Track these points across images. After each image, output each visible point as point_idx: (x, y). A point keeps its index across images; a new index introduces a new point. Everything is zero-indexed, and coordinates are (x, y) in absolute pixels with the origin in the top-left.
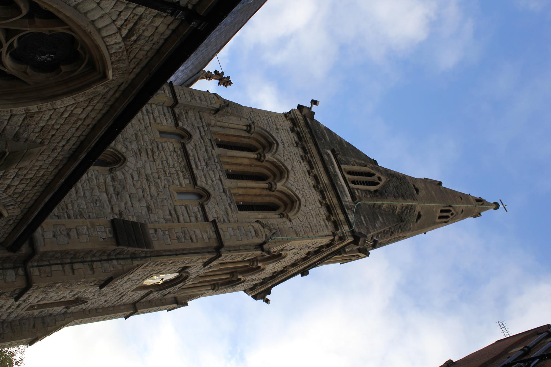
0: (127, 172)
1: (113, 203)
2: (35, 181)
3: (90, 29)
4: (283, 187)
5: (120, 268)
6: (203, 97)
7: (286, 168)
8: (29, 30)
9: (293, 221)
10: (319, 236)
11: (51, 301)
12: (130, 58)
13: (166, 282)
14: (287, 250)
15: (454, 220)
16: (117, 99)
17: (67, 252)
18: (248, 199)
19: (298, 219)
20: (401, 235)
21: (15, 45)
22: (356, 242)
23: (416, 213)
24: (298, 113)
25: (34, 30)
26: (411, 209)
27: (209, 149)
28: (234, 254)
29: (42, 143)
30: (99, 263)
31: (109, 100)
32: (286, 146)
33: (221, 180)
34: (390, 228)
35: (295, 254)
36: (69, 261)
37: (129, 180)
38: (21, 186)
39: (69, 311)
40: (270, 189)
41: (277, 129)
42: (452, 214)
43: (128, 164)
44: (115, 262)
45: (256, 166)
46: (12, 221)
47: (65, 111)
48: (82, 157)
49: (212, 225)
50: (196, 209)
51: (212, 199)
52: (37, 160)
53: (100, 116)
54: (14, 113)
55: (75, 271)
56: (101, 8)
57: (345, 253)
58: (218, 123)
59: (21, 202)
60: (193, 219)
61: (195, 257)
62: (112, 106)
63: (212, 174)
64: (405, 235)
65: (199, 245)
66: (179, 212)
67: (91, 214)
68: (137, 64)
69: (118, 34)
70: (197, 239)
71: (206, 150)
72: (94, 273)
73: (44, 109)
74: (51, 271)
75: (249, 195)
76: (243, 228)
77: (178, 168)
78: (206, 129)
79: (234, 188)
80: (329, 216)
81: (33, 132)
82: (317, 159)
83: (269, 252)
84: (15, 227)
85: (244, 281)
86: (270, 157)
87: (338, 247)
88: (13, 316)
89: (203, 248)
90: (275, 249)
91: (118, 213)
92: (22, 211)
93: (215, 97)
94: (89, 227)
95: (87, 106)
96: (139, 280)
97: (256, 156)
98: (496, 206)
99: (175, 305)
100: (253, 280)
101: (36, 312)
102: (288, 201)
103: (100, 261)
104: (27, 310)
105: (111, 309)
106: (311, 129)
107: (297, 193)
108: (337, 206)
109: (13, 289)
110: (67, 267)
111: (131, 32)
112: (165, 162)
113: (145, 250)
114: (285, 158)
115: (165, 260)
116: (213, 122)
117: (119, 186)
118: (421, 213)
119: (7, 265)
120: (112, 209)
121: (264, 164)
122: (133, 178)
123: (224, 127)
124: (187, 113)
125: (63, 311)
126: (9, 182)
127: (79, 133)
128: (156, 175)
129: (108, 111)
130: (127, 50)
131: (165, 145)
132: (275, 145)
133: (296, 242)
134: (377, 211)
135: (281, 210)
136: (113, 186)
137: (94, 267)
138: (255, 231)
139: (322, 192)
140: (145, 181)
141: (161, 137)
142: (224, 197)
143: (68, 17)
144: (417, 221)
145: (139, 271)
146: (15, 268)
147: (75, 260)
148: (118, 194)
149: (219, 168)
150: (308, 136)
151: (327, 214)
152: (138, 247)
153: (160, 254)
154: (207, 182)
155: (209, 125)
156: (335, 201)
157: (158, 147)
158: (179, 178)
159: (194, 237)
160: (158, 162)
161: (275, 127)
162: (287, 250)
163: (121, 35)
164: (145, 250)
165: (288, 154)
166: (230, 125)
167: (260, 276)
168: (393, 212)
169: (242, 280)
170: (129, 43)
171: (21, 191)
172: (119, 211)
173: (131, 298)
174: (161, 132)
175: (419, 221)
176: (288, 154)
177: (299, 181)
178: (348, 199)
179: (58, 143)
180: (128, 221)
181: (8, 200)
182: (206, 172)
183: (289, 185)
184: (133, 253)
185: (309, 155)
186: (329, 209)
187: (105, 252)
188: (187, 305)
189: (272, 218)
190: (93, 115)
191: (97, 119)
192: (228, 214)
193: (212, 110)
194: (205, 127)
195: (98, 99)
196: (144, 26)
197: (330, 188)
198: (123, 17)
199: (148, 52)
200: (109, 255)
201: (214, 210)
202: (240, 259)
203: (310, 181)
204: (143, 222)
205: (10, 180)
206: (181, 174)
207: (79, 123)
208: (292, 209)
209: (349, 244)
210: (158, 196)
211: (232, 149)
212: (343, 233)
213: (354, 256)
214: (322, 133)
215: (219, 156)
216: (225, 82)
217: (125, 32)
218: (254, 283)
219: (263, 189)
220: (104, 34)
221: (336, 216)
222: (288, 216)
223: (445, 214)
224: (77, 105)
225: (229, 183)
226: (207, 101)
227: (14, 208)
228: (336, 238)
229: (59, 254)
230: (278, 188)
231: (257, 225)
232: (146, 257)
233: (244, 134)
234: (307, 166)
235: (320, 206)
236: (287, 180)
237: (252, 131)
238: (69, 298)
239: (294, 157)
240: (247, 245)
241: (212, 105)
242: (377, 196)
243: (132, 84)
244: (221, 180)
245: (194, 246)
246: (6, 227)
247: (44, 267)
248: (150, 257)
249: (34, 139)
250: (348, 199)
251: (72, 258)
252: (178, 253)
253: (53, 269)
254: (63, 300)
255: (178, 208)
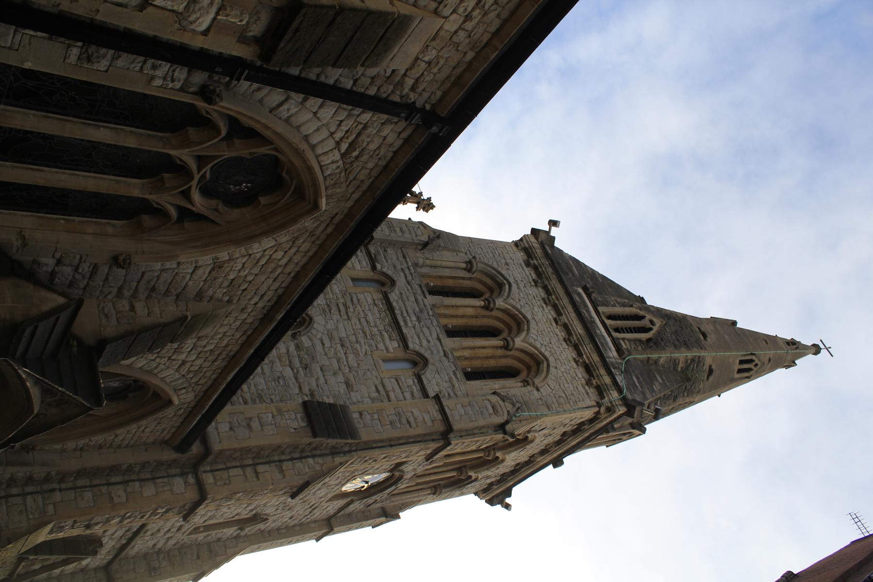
0: (315, 336)
1: (301, 380)
2: (217, 353)
3: (303, 146)
4: (523, 344)
5: (318, 468)
6: (405, 228)
7: (525, 317)
8: (227, 154)
9: (541, 390)
10: (579, 409)
11: (221, 520)
12: (349, 180)
13: (372, 487)
14: (535, 431)
15: (759, 374)
16: (329, 236)
17: (247, 450)
18: (477, 363)
19: (548, 386)
20: (687, 400)
21: (208, 176)
22: (630, 413)
23: (706, 367)
24: (533, 239)
25: (233, 154)
26: (699, 362)
27: (420, 298)
28: (467, 441)
29: (229, 302)
30: (290, 463)
31: (318, 238)
32: (521, 286)
33: (440, 340)
34: (672, 391)
35: (546, 436)
36: (250, 462)
37: (319, 347)
38: (198, 362)
39: (242, 534)
40: (506, 347)
41: (507, 264)
42: (756, 365)
43: (315, 325)
44: (310, 460)
45: (484, 317)
46: (182, 411)
47: (263, 256)
48: (279, 317)
49: (434, 403)
50: (410, 382)
51: (430, 367)
52: (222, 325)
53: (305, 260)
54: (200, 263)
55: (260, 476)
56: (318, 118)
57: (614, 430)
58: (428, 262)
59: (197, 383)
60: (408, 395)
61: (415, 448)
62: (321, 246)
63: (427, 332)
64: (692, 400)
65: (420, 431)
66: (389, 387)
67: (273, 397)
68: (357, 188)
69: (337, 150)
70: (416, 423)
71: (416, 299)
72: (284, 477)
73: (237, 256)
74: (229, 476)
75: (478, 358)
76: (475, 404)
77: (381, 327)
78: (413, 271)
79: (458, 350)
80: (590, 380)
81: (220, 287)
82: (565, 301)
83: (512, 435)
84: (185, 419)
85: (476, 480)
86: (501, 303)
87: (605, 423)
88: (172, 542)
89: (425, 435)
90: (520, 431)
91: (308, 393)
92: (196, 396)
93: (421, 227)
94: (275, 414)
95: (290, 249)
96: (337, 485)
97: (482, 303)
98: (816, 349)
99: (383, 519)
100: (488, 477)
101: (201, 537)
102: (532, 363)
103: (292, 459)
104: (190, 534)
105: (297, 528)
106: (552, 261)
107: (543, 350)
108: (599, 365)
109: (181, 503)
110: (249, 470)
111: (352, 146)
112: (363, 320)
113: (350, 441)
114: (522, 303)
115: (376, 453)
116: (421, 261)
117: (306, 356)
118: (713, 367)
119: (173, 471)
120: (300, 388)
121: (495, 313)
122: (323, 344)
123: (435, 267)
124: (385, 250)
125: (235, 534)
126: (183, 356)
127: (277, 284)
128: (353, 338)
129: (315, 253)
130: (346, 170)
131: (361, 296)
132: (507, 286)
133: (548, 418)
134: (653, 367)
135: (523, 375)
136: (299, 356)
137: (284, 468)
138: (493, 407)
139: (576, 347)
140: (339, 347)
141: (354, 286)
142: (446, 363)
143: (277, 134)
144: (708, 378)
145: (340, 473)
146: (182, 474)
147: (258, 461)
148: (306, 368)
149: (435, 323)
150: (550, 270)
151: (586, 376)
152: (341, 438)
153: (369, 446)
154: (421, 343)
155: (416, 265)
156: (596, 358)
157: (352, 300)
158: (383, 340)
159: (412, 420)
160: (354, 320)
161: (503, 261)
162: (535, 431)
163: (339, 151)
164: (350, 441)
165: (525, 296)
166: (444, 264)
167: (497, 471)
168: (675, 368)
169: (473, 478)
170: (349, 161)
171: (197, 368)
172: (310, 390)
173: (325, 512)
174: (354, 280)
175: (711, 378)
176: (525, 296)
177: (543, 334)
178: (612, 354)
179: (250, 300)
180: (325, 403)
181: (180, 381)
182: (418, 330)
183: (531, 340)
184: (333, 447)
185: (554, 297)
186: (588, 369)
187: (297, 447)
188: (399, 518)
189: (512, 387)
190: (296, 259)
191: (301, 264)
192: (453, 386)
193: (418, 244)
194: (411, 268)
195: (305, 236)
196: (368, 137)
197: (587, 340)
198: (344, 128)
199: (371, 170)
200: (303, 451)
201: (434, 382)
202: (474, 448)
203: (558, 333)
204: (342, 403)
205: (185, 355)
206: (386, 334)
207: (279, 270)
208: (538, 372)
209: (619, 418)
210: (358, 367)
211: (448, 296)
212: (611, 402)
213: (625, 434)
214: (568, 264)
215: (434, 306)
216: (426, 205)
217: (344, 147)
218: (489, 481)
219: (497, 347)
220: (319, 151)
221: (599, 379)
222: (534, 383)
223: (746, 366)
224: (277, 247)
225: (451, 343)
226: (410, 233)
227: (187, 392)
228: (603, 409)
229: (239, 453)
230: (516, 346)
231: (494, 399)
232: (350, 451)
233: (462, 274)
234: (553, 313)
235: (575, 365)
236: (528, 333)
237: (474, 269)
238: (245, 514)
239: (534, 301)
240: (483, 427)
241: (418, 238)
242: (651, 347)
243: (349, 215)
244: (440, 340)
245: (413, 432)
246: (174, 419)
247: (219, 473)
248: (356, 450)
249: (220, 296)
250: (612, 354)
251: (254, 458)
252: (393, 443)
253: (231, 474)
254: (237, 518)
255: (387, 382)
